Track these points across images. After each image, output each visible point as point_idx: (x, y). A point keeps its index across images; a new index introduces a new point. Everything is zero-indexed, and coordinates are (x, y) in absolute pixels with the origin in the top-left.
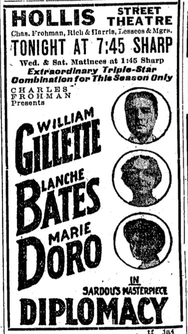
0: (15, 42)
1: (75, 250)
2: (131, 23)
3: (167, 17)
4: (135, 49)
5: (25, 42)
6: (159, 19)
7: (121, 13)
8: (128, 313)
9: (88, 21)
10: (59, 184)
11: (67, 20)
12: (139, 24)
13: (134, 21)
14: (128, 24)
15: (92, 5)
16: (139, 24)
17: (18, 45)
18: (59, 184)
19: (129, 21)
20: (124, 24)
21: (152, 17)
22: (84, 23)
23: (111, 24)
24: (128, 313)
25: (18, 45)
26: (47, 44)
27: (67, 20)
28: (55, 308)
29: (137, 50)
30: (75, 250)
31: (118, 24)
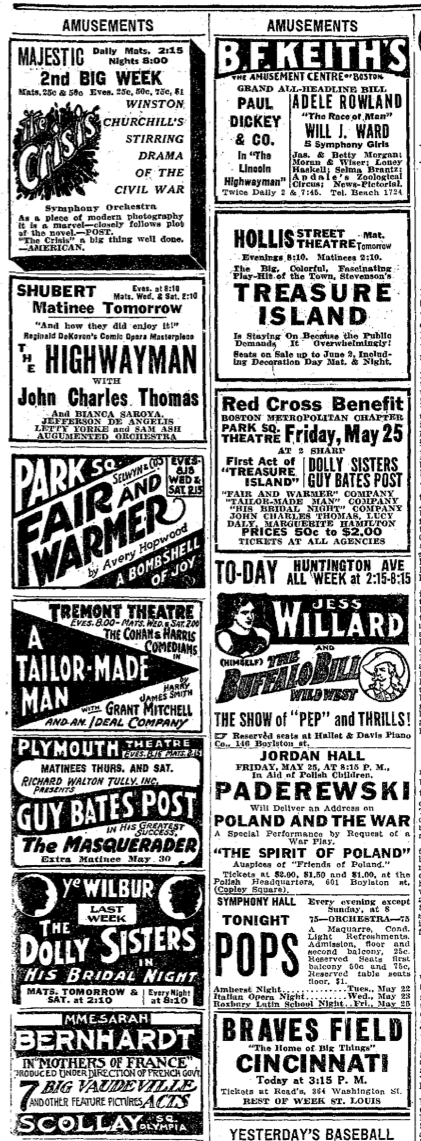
0: (219, 563)
1: (93, 538)
2: (283, 794)
3: (244, 850)
4: (295, 943)
5: (227, 580)
6: (362, 289)
7: (277, 320)
8: (71, 557)
9: (277, 320)
10: (141, 493)
11: (299, 318)
12: (315, 324)
13: (322, 244)
14: (359, 825)
15: (205, 406)
16: (315, 324)
17: (224, 567)
18: (141, 493)
19: (359, 821)
20: (352, 825)
21: (247, 286)
22: (273, 322)
23: (227, 923)
24: (71, 557)
25: (224, 567)
26: (79, 353)
27: (299, 318)
28: (89, 540)
29: (290, 941)
30: (93, 538)
31: (345, 825)
